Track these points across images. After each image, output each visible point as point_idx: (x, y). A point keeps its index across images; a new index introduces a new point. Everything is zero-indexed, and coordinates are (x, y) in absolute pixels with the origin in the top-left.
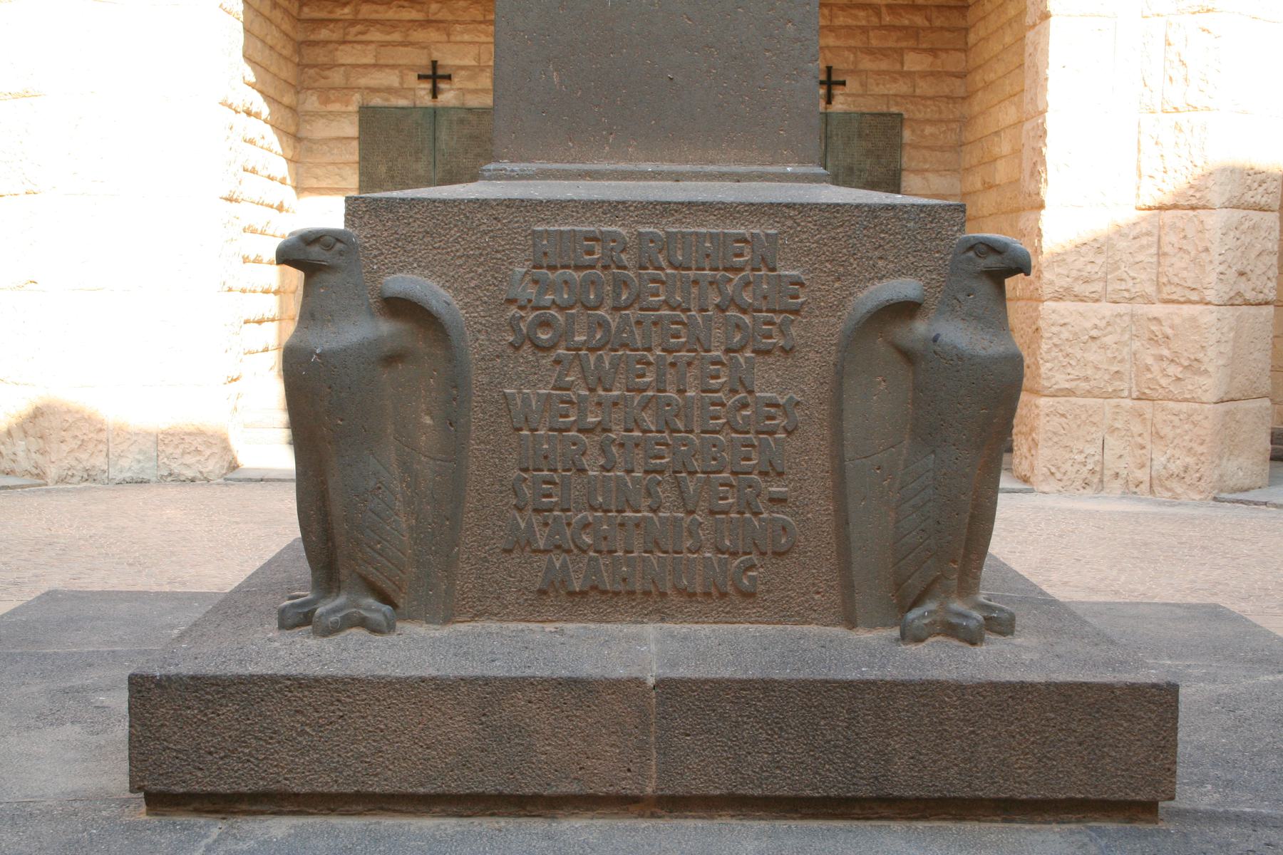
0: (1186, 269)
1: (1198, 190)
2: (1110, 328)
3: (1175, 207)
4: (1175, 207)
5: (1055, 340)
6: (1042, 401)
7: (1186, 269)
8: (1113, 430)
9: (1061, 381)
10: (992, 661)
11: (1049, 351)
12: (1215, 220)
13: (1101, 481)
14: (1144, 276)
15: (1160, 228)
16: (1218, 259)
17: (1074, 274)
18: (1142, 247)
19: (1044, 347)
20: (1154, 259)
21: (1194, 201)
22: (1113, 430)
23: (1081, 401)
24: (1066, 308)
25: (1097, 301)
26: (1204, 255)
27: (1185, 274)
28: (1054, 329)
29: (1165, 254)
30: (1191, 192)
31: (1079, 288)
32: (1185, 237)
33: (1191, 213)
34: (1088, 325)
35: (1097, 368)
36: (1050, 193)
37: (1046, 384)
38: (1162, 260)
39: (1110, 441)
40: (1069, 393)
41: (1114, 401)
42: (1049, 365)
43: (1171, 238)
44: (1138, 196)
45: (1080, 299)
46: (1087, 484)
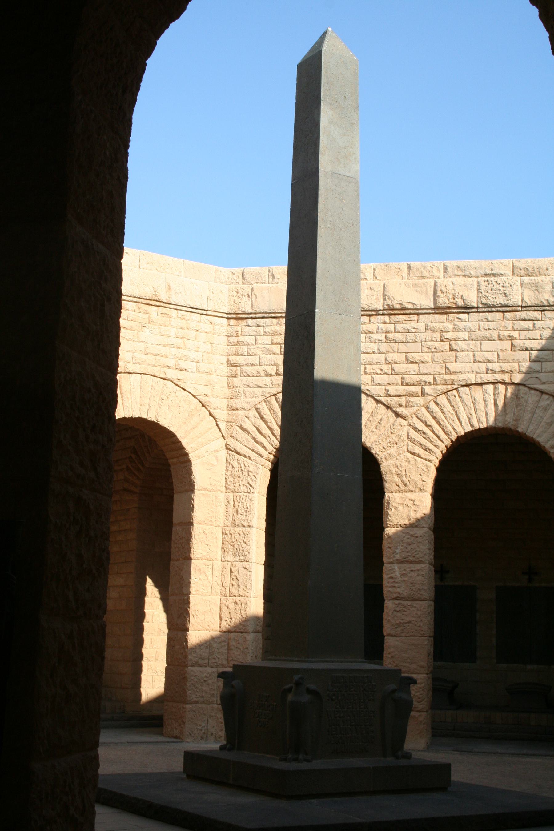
0: (239, 655)
1: (244, 626)
2: (210, 677)
3: (235, 632)
4: (235, 632)
5: (192, 682)
6: (187, 706)
7: (239, 655)
8: (211, 716)
9: (194, 698)
10: (403, 762)
11: (190, 686)
12: (250, 637)
13: (207, 737)
14: (223, 657)
15: (229, 639)
16: (251, 651)
17: (199, 656)
18: (222, 647)
19: (188, 685)
20: (226, 651)
21: (242, 630)
22: (211, 716)
23: (200, 705)
24: (195, 669)
25: (206, 667)
26: (246, 650)
27: (239, 657)
28: (192, 678)
29: (231, 649)
30: (241, 627)
31: (200, 662)
32: (239, 643)
33: (241, 634)
34: (203, 676)
35: (206, 693)
36: (191, 627)
37: (189, 699)
38: (229, 651)
39: (210, 720)
40: (197, 702)
41: (211, 705)
42: (190, 692)
43: (233, 643)
44: (220, 627)
45: (200, 666)
46: (202, 738)
